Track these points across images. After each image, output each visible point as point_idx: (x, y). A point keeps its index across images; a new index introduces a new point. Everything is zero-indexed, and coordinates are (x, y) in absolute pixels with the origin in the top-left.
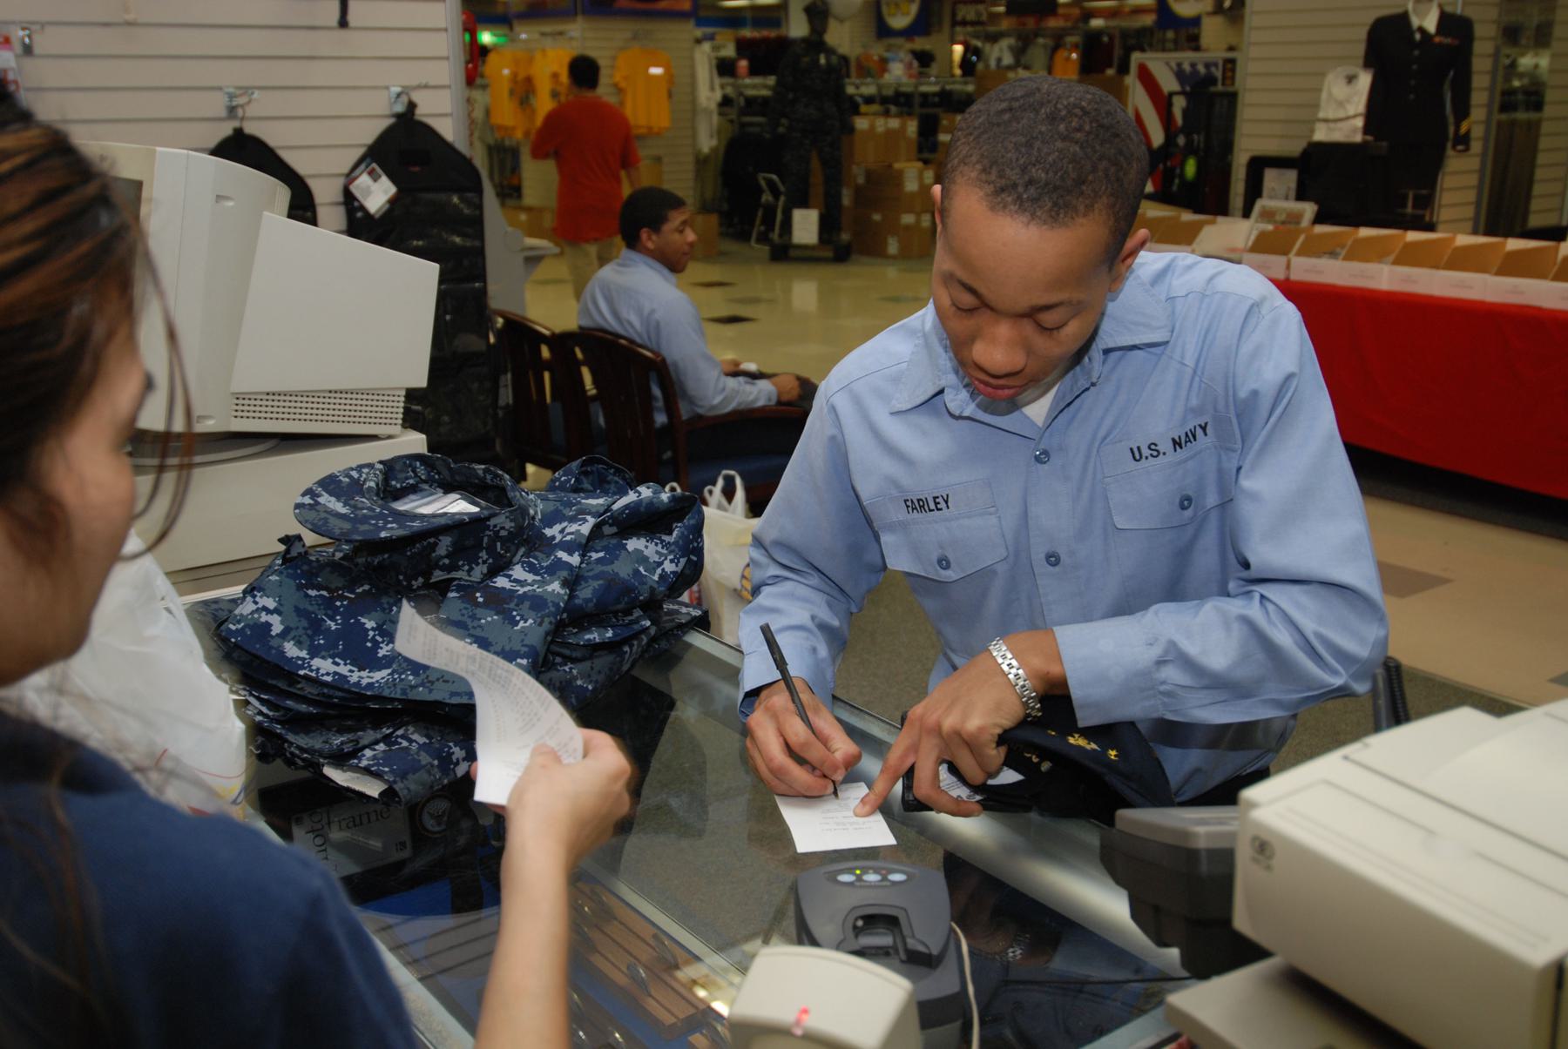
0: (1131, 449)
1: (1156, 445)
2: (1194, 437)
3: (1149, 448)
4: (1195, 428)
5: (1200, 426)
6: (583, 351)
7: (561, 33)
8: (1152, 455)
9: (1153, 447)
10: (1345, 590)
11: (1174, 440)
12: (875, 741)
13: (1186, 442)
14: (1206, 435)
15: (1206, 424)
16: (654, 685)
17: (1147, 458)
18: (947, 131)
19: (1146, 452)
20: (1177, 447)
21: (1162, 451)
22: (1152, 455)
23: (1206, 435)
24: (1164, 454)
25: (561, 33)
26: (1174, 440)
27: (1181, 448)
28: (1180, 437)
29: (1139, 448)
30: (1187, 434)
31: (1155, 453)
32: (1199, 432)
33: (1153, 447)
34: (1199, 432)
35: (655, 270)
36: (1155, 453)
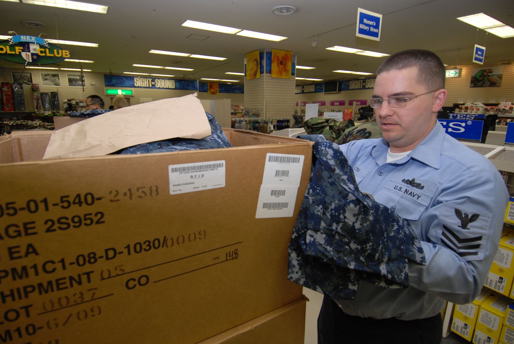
4: (416, 194)
7: (214, 186)
8: (399, 190)
13: (409, 194)
15: (420, 196)
24: (401, 191)
27: (407, 193)
28: (408, 191)
29: (398, 186)
36: (400, 190)
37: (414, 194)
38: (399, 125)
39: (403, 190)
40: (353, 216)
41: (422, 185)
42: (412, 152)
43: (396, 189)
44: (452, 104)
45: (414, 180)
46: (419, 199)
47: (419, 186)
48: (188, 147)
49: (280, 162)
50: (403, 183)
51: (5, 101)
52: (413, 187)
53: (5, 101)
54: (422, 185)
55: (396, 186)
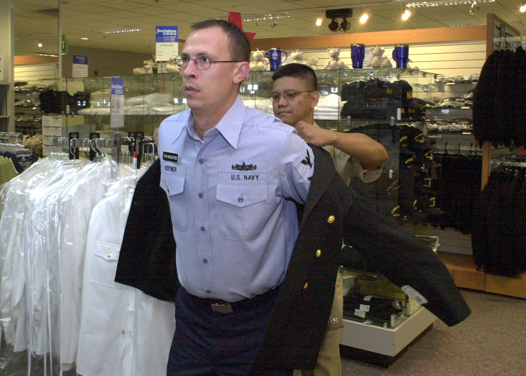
0: (232, 175)
1: (239, 176)
2: (253, 179)
3: (237, 176)
4: (254, 176)
5: (256, 176)
6: (29, 100)
7: (172, 45)
8: (237, 179)
9: (238, 176)
10: (406, 355)
11: (245, 176)
12: (19, 303)
13: (249, 178)
14: (257, 179)
15: (258, 176)
16: (427, 29)
17: (236, 179)
18: (336, 67)
19: (236, 177)
20: (245, 179)
21: (240, 179)
22: (237, 179)
23: (257, 179)
24: (241, 180)
25: (172, 45)
26: (245, 176)
27: (247, 179)
28: (247, 176)
29: (234, 176)
30: (250, 176)
31: (238, 179)
32: (255, 178)
33: (238, 176)
34: (255, 178)
35: (286, 247)
36: (238, 179)
37: (253, 176)
38: (312, 74)
39: (242, 177)
40: (25, 349)
41: (254, 165)
42: (154, 106)
43: (235, 180)
44: (227, 14)
45: (244, 164)
46: (258, 178)
47: (251, 167)
48: (58, 189)
49: (149, 152)
50: (234, 171)
51: (433, 137)
52: (247, 171)
53: (433, 137)
54: (254, 165)
55: (232, 175)
